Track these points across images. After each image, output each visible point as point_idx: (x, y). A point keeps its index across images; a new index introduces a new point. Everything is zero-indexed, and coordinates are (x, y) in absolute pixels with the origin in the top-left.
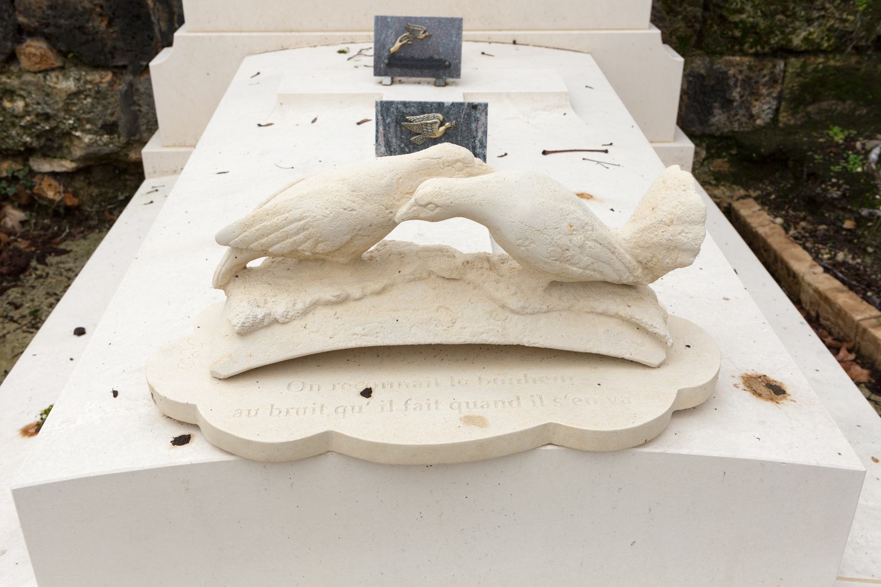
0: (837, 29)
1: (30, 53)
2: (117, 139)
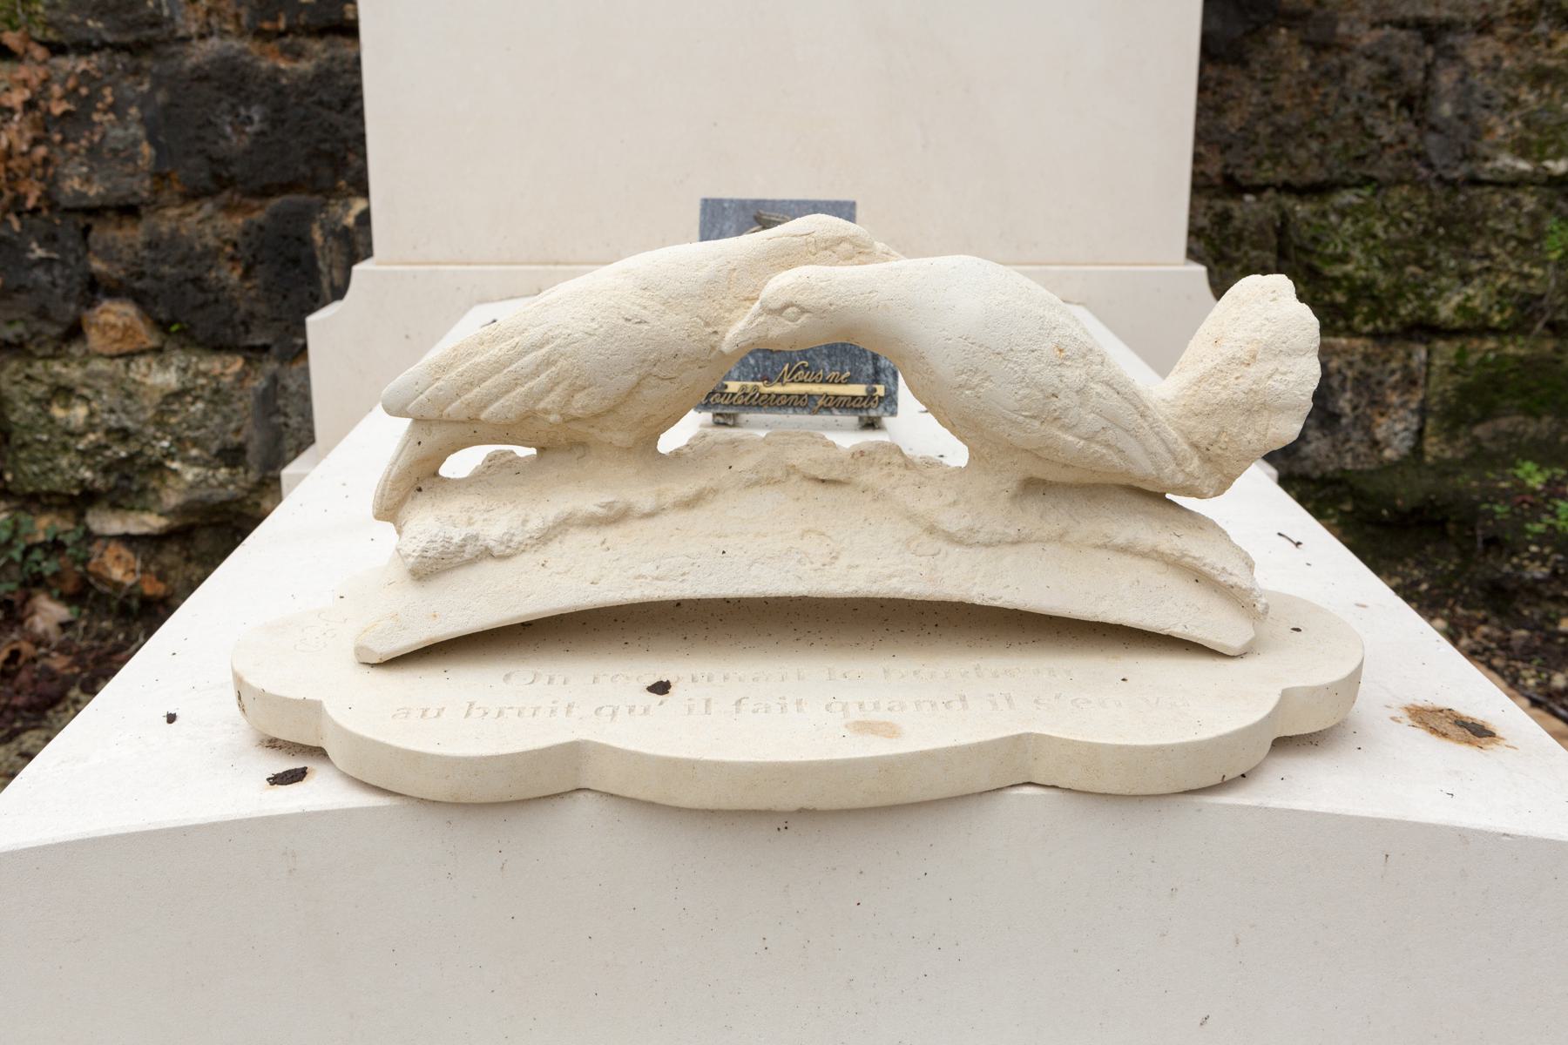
0: (1515, 291)
1: (106, 324)
2: (242, 476)
